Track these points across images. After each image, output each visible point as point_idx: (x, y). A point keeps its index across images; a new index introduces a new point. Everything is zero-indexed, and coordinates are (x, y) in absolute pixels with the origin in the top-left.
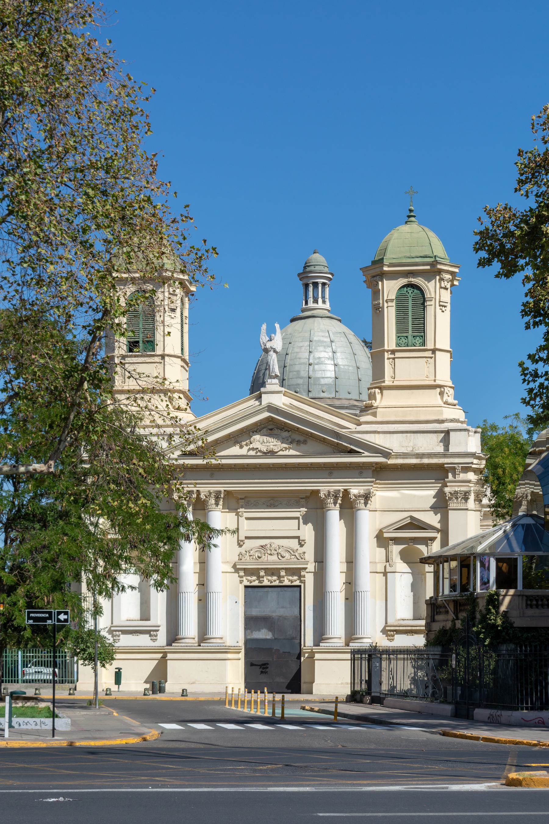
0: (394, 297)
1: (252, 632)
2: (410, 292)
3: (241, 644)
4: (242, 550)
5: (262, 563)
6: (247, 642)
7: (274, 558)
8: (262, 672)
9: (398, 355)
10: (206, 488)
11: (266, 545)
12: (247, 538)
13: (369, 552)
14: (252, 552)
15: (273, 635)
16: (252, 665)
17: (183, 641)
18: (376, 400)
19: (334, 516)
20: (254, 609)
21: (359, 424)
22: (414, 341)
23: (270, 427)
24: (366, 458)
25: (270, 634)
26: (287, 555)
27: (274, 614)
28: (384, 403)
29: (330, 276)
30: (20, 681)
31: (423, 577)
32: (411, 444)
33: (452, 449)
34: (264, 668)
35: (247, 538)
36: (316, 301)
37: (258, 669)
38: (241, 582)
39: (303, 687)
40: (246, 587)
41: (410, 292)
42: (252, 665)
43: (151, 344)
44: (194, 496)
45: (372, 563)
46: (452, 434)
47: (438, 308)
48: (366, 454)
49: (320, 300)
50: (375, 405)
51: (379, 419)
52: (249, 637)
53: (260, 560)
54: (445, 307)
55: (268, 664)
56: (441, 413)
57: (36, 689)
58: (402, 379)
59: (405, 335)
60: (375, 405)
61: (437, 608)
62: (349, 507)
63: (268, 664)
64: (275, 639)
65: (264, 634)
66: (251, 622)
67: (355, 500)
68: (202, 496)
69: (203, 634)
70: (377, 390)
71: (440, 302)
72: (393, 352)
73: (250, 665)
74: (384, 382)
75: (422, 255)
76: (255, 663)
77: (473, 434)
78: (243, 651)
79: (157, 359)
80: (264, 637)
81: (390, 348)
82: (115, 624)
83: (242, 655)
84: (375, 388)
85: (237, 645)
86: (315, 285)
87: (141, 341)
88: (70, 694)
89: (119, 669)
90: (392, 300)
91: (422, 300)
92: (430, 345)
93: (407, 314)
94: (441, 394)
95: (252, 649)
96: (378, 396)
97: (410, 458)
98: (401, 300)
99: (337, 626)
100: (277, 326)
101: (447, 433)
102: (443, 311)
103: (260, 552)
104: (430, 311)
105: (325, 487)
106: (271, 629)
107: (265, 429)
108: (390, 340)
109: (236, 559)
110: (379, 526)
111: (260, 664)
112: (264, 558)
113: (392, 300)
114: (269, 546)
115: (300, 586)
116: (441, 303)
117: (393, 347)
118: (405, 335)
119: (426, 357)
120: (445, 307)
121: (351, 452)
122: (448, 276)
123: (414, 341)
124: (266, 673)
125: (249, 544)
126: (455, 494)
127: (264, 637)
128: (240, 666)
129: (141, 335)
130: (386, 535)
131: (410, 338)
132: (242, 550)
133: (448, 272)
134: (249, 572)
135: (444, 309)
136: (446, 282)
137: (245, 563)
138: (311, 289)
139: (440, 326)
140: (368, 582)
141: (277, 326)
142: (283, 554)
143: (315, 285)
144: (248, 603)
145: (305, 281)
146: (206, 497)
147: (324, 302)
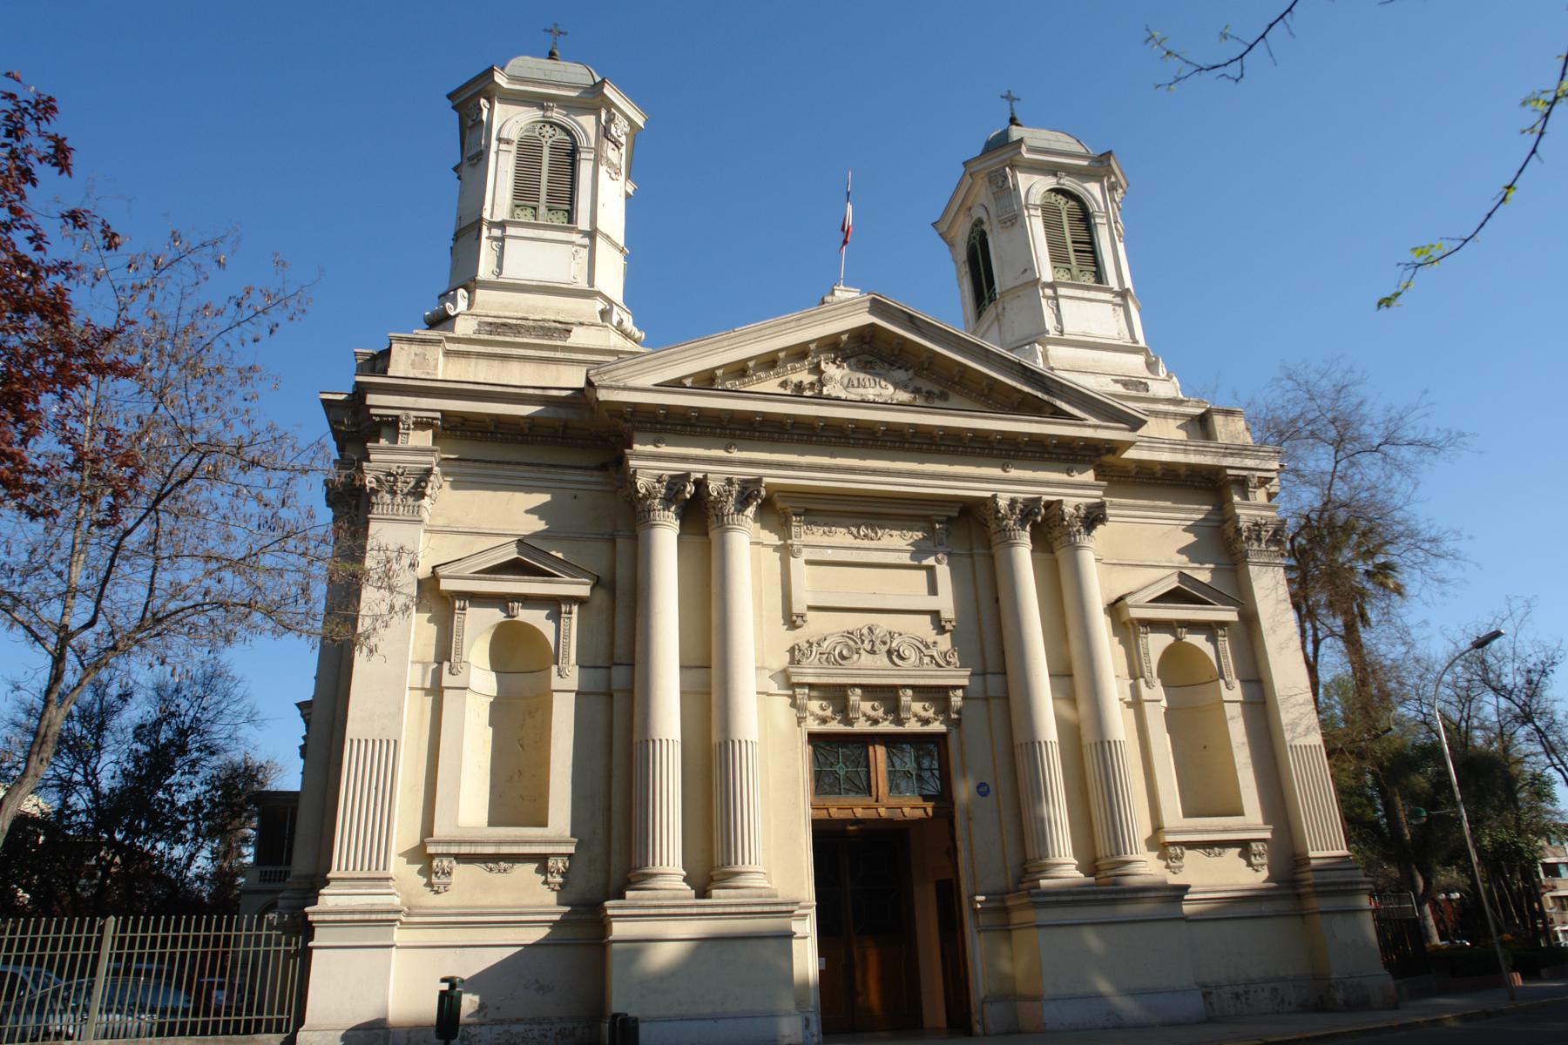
4: (799, 636)
9: (510, 231)
10: (718, 466)
12: (811, 608)
14: (825, 645)
19: (666, 537)
24: (1092, 429)
35: (811, 608)
40: (813, 738)
44: (690, 488)
48: (1092, 421)
62: (1052, 531)
67: (374, 491)
72: (502, 225)
78: (813, 912)
81: (497, 219)
91: (1085, 218)
92: (583, 223)
97: (1161, 450)
105: (1003, 485)
117: (502, 214)
125: (817, 625)
126: (390, 481)
134: (836, 695)
139: (608, 195)
144: (823, 782)
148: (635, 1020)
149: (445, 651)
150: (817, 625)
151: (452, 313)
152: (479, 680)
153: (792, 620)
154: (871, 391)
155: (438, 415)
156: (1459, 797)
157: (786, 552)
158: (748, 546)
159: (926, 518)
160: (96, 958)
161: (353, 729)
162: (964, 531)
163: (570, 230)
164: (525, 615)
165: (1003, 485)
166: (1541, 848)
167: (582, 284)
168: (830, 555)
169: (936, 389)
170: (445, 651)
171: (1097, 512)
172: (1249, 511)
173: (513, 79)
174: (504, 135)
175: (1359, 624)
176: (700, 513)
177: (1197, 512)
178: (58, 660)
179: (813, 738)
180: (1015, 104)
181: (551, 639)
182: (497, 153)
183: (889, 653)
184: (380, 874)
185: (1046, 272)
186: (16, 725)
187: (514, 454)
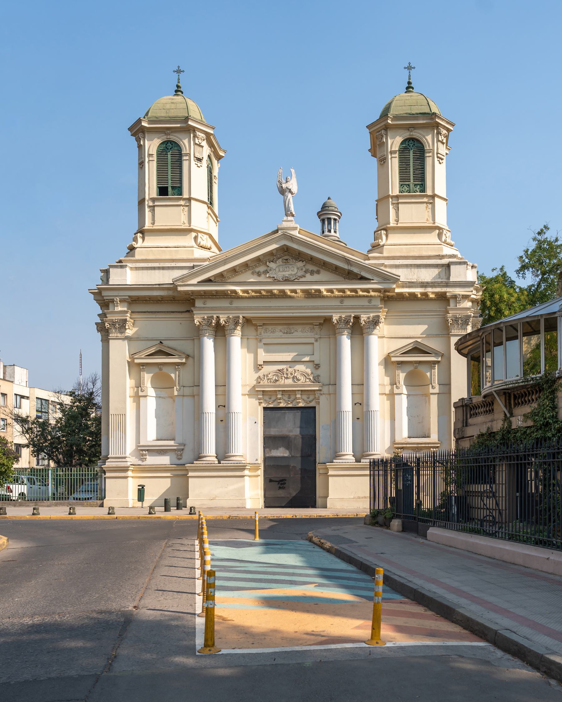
0: (397, 149)
1: (270, 451)
2: (411, 145)
3: (261, 461)
4: (261, 373)
5: (279, 386)
6: (266, 459)
7: (290, 381)
8: (280, 488)
11: (283, 369)
13: (378, 377)
14: (270, 376)
15: (290, 453)
16: (271, 481)
17: (204, 459)
18: (382, 240)
20: (272, 429)
21: (369, 259)
22: (415, 189)
23: (285, 258)
25: (288, 452)
26: (302, 379)
27: (291, 434)
28: (390, 241)
29: (339, 214)
30: (50, 499)
31: (427, 398)
32: (415, 277)
33: (452, 279)
34: (282, 484)
36: (329, 231)
37: (276, 485)
38: (260, 403)
39: (319, 501)
40: (265, 409)
41: (411, 145)
42: (271, 481)
43: (178, 190)
45: (382, 385)
46: (452, 267)
47: (436, 159)
49: (332, 231)
50: (381, 244)
51: (385, 254)
52: (267, 455)
53: (278, 383)
54: (442, 159)
55: (285, 480)
56: (442, 250)
57: (34, 509)
58: (405, 221)
59: (407, 183)
60: (381, 244)
61: (471, 409)
63: (285, 480)
64: (292, 457)
65: (281, 452)
66: (270, 441)
68: (222, 321)
69: (223, 453)
70: (383, 232)
71: (437, 153)
72: (397, 197)
73: (269, 481)
74: (389, 223)
75: (421, 112)
76: (273, 479)
77: (470, 268)
79: (182, 203)
80: (282, 455)
81: (394, 194)
82: (141, 444)
83: (261, 472)
84: (381, 230)
85: (256, 462)
86: (329, 219)
87: (170, 185)
88: (70, 514)
89: (143, 487)
90: (395, 152)
92: (429, 192)
93: (409, 165)
94: (440, 236)
95: (271, 465)
96: (384, 237)
98: (403, 150)
99: (348, 447)
100: (293, 171)
101: (448, 266)
102: (440, 163)
103: (277, 376)
104: (428, 161)
106: (288, 447)
107: (280, 260)
108: (394, 189)
109: (255, 383)
110: (386, 352)
111: (278, 480)
112: (282, 382)
113: (395, 152)
114: (285, 370)
115: (314, 408)
116: (439, 155)
117: (396, 192)
118: (407, 183)
119: (424, 203)
120: (442, 159)
121: (363, 278)
122: (444, 132)
123: (415, 189)
124: (283, 488)
125: (267, 369)
127: (281, 455)
128: (260, 481)
129: (170, 181)
130: (393, 359)
131: (412, 186)
132: (261, 373)
133: (444, 127)
135: (441, 161)
136: (442, 137)
137: (263, 386)
138: (326, 222)
140: (378, 403)
141: (293, 171)
142: (299, 377)
143: (329, 219)
145: (322, 217)
146: (225, 322)
147: (335, 232)
151: (136, 246)
154: (287, 273)
155: (127, 298)
159: (312, 324)
160: (48, 474)
161: (111, 412)
163: (180, 199)
166: (60, 429)
167: (186, 226)
169: (315, 268)
170: (139, 385)
171: (377, 319)
173: (150, 122)
174: (150, 153)
176: (221, 332)
179: (265, 409)
180: (412, 71)
181: (174, 378)
182: (148, 162)
183: (293, 378)
184: (124, 456)
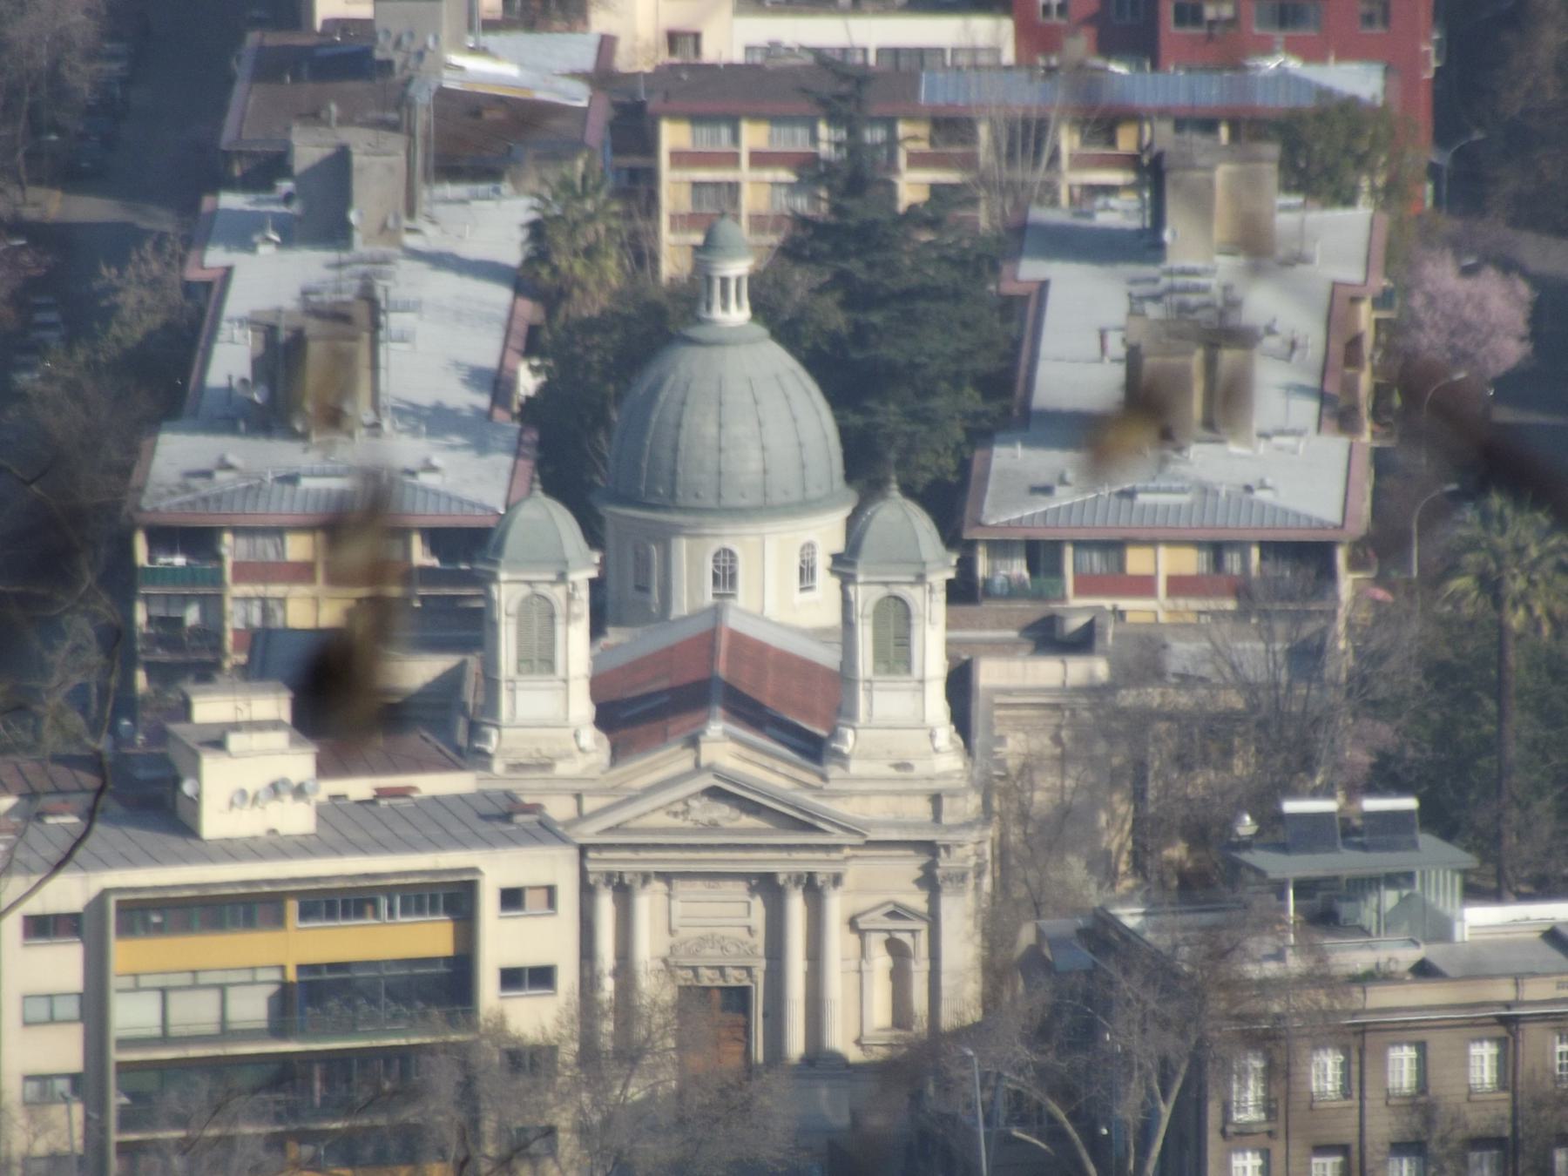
4: (674, 940)
92: (916, 672)
148: (1102, 908)
149: (863, 952)
150: (684, 933)
152: (881, 962)
153: (671, 932)
156: (1372, 804)
157: (669, 896)
158: (647, 904)
162: (769, 888)
164: (899, 936)
165: (782, 866)
168: (693, 897)
170: (863, 952)
172: (945, 863)
175: (1235, 854)
177: (923, 859)
178: (1379, 906)
185: (1122, 868)
186: (230, 378)
187: (785, 737)
